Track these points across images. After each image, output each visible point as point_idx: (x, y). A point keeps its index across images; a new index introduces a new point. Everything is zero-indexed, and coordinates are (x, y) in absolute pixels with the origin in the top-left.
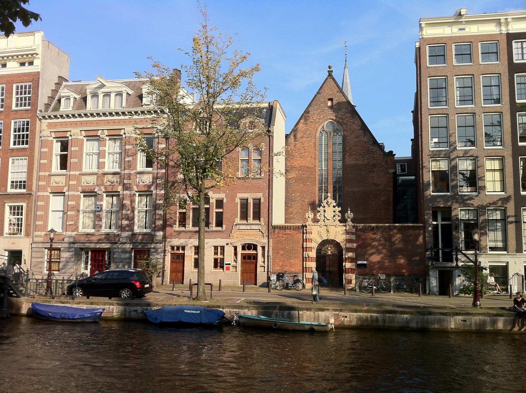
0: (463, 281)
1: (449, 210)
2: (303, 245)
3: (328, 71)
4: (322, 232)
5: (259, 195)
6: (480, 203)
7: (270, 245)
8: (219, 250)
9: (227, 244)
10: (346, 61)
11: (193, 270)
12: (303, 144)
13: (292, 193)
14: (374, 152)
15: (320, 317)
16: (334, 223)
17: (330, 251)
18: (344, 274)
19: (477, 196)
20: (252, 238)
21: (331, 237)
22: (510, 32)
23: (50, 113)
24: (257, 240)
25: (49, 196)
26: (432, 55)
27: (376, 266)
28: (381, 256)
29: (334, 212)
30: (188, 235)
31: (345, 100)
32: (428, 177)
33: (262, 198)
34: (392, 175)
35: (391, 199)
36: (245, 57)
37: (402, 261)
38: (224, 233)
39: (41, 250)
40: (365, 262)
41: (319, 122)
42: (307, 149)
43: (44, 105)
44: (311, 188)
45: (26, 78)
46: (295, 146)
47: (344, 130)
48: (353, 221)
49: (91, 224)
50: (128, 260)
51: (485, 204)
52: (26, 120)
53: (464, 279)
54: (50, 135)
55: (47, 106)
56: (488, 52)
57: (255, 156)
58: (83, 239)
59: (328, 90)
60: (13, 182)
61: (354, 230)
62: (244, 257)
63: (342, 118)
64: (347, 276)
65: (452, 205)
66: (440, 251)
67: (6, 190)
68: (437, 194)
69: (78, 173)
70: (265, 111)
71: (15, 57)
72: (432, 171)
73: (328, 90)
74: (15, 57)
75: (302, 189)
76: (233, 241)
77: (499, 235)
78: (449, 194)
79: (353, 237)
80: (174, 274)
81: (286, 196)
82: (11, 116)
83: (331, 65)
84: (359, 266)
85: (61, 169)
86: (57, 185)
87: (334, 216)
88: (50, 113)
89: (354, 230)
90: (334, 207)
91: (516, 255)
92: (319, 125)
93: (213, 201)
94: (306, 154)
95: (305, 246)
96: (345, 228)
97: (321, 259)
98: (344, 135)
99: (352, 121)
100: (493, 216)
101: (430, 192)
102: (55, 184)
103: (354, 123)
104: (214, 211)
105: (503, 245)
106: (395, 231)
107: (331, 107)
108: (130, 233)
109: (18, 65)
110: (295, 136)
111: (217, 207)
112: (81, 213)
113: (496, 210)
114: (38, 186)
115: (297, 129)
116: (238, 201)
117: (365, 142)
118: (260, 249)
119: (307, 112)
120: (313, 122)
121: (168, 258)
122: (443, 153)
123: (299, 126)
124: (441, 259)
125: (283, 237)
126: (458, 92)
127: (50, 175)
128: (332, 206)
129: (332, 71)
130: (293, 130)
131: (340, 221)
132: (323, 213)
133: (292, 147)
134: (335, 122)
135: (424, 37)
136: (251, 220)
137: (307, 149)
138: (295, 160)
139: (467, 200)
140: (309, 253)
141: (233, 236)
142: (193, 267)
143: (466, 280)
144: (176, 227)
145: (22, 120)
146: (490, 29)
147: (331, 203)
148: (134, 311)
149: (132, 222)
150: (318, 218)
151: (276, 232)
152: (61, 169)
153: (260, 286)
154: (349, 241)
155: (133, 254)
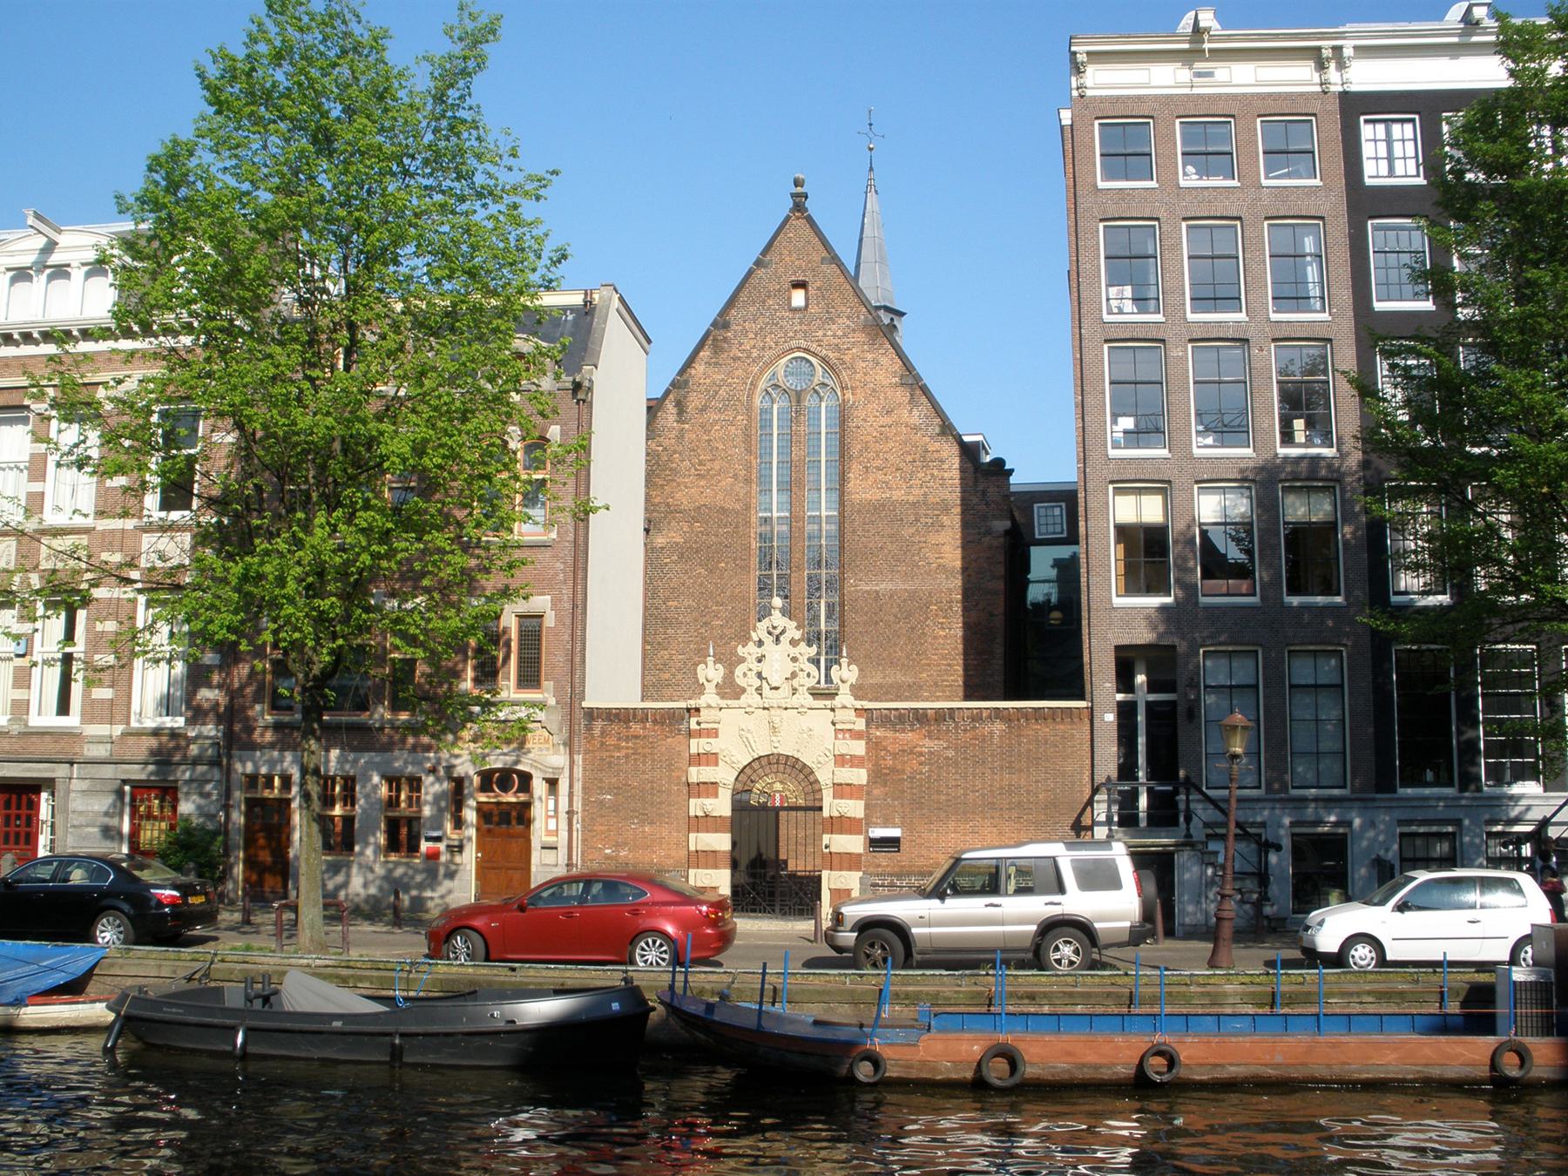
3: (793, 195)
7: (575, 775)
10: (871, 169)
13: (668, 599)
14: (942, 461)
17: (779, 790)
21: (786, 747)
22: (1354, 88)
26: (1112, 151)
29: (794, 659)
33: (548, 611)
34: (1002, 540)
35: (999, 621)
41: (759, 357)
42: (721, 447)
44: (735, 582)
46: (680, 437)
48: (858, 691)
56: (1283, 147)
59: (790, 255)
63: (837, 348)
70: (570, 317)
73: (790, 255)
75: (701, 585)
78: (1339, 599)
81: (646, 609)
83: (801, 176)
84: (877, 844)
87: (794, 675)
90: (794, 643)
91: (1373, 800)
96: (700, 719)
99: (869, 356)
103: (878, 363)
115: (686, 382)
117: (916, 428)
118: (539, 787)
120: (739, 358)
123: (693, 372)
125: (619, 748)
128: (785, 639)
130: (673, 384)
131: (816, 694)
133: (669, 440)
135: (1089, 93)
137: (721, 447)
138: (679, 484)
146: (1297, 77)
147: (783, 632)
150: (740, 681)
151: (597, 732)
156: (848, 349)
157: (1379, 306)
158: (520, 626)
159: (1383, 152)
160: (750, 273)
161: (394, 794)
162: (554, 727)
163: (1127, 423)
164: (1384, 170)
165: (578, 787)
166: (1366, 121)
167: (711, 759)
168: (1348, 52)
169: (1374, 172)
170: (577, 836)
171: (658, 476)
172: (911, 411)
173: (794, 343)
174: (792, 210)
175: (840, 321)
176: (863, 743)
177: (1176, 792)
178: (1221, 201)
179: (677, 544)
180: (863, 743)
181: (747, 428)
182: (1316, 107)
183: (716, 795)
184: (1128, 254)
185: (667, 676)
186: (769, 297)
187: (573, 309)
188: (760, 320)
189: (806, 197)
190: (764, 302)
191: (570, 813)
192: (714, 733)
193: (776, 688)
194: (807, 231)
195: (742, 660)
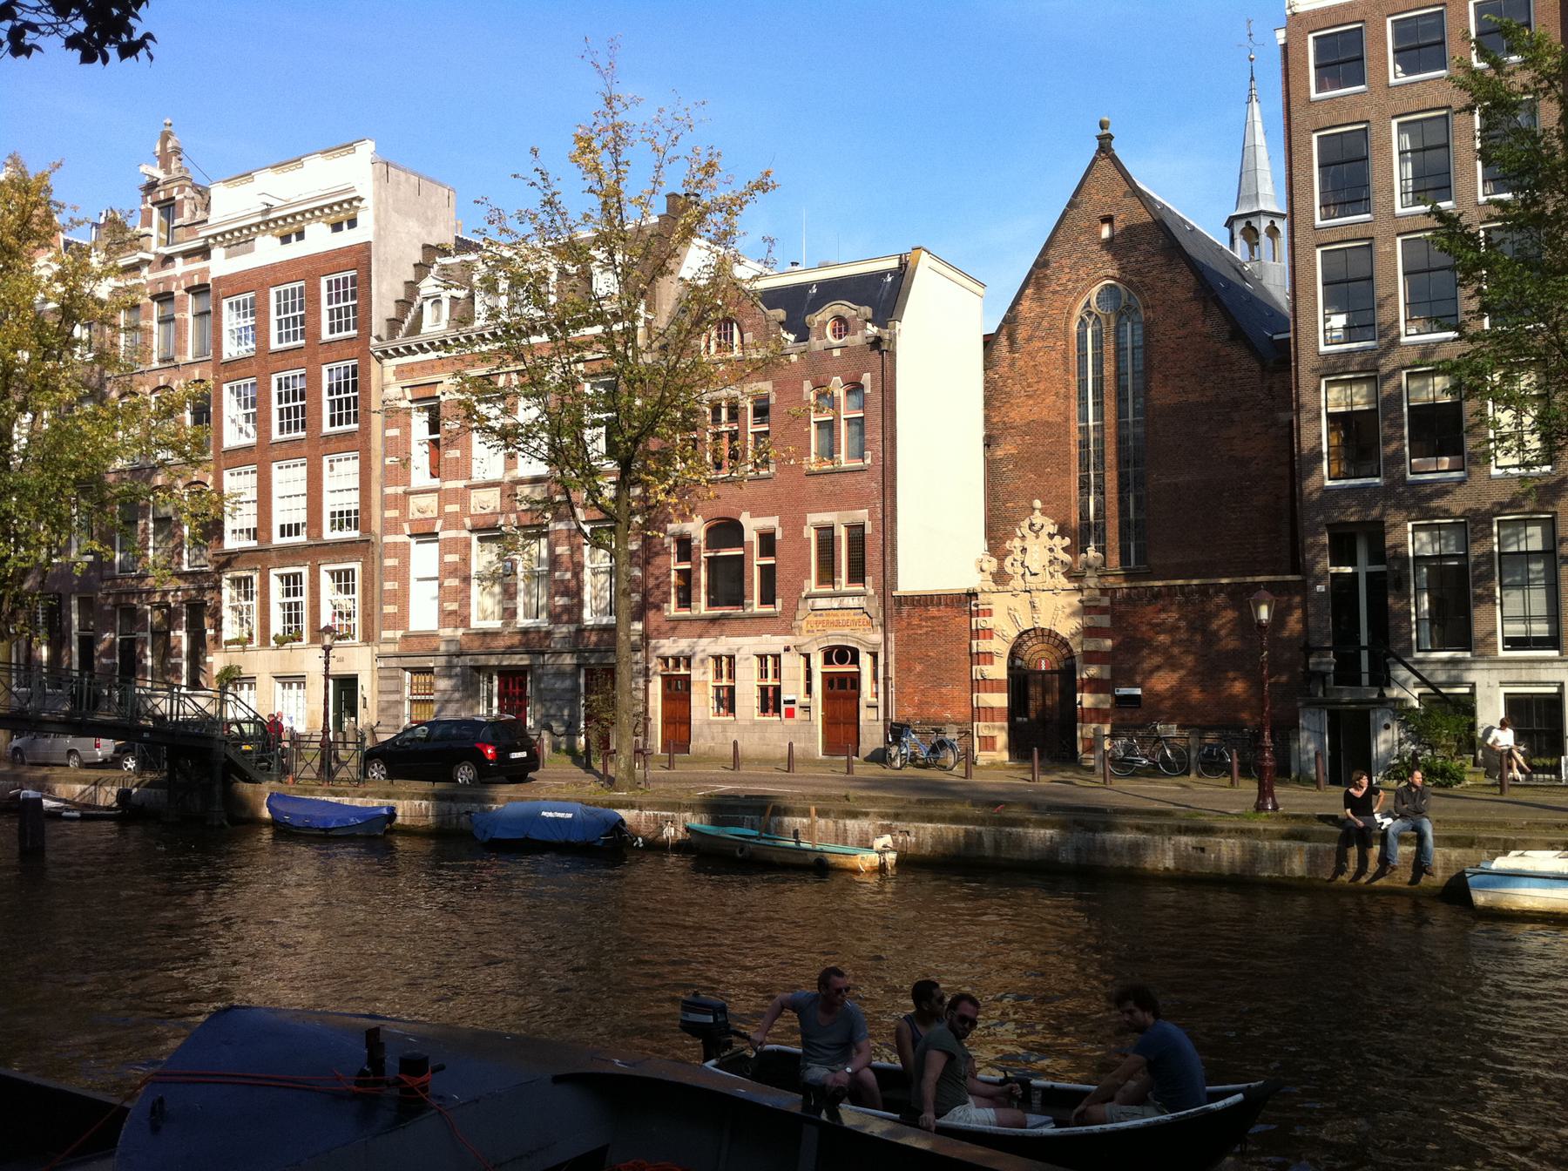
0: (1401, 742)
1: (1376, 532)
2: (970, 645)
3: (1099, 138)
4: (1018, 608)
5: (862, 515)
6: (1471, 505)
8: (769, 663)
9: (787, 649)
10: (1252, 79)
11: (756, 718)
12: (1033, 358)
13: (1006, 501)
14: (1232, 364)
15: (849, 833)
16: (1050, 583)
17: (1042, 660)
18: (1079, 724)
19: (1461, 482)
20: (846, 631)
21: (1044, 623)
23: (401, 340)
24: (858, 635)
25: (407, 544)
27: (1168, 703)
28: (1183, 672)
29: (1051, 550)
30: (698, 627)
31: (1146, 218)
32: (1320, 436)
36: (711, 165)
37: (1238, 687)
38: (780, 621)
39: (394, 674)
40: (1138, 691)
41: (1074, 288)
42: (1045, 370)
43: (385, 324)
45: (343, 261)
46: (1012, 365)
47: (1146, 307)
49: (497, 610)
50: (568, 696)
51: (1488, 506)
52: (350, 363)
53: (1402, 735)
54: (401, 395)
55: (394, 324)
57: (847, 410)
58: (476, 645)
60: (333, 514)
61: (1106, 602)
62: (828, 679)
63: (1138, 272)
64: (1085, 731)
65: (1383, 514)
66: (1364, 655)
67: (269, 540)
68: (1342, 482)
69: (461, 484)
70: (889, 279)
71: (317, 213)
72: (1332, 417)
74: (317, 213)
76: (800, 640)
77: (1538, 600)
78: (1377, 480)
79: (1105, 621)
80: (672, 728)
82: (321, 357)
83: (1106, 119)
84: (1121, 701)
85: (433, 476)
86: (422, 516)
88: (401, 340)
90: (1051, 536)
92: (1076, 300)
93: (751, 535)
94: (1042, 386)
95: (974, 650)
97: (1020, 681)
99: (1167, 276)
100: (1518, 542)
101: (1325, 477)
102: (418, 515)
104: (757, 561)
105: (1550, 632)
106: (1221, 599)
107: (1108, 244)
108: (572, 628)
109: (278, 241)
110: (1012, 339)
111: (763, 554)
112: (474, 583)
113: (1526, 523)
114: (384, 521)
115: (1015, 317)
116: (812, 534)
118: (865, 661)
119: (1041, 264)
120: (1057, 292)
121: (656, 687)
122: (1358, 359)
123: (1021, 308)
124: (1365, 679)
125: (921, 627)
126: (1410, 165)
127: (407, 494)
129: (1111, 137)
130: (1004, 320)
132: (1018, 555)
133: (1003, 369)
134: (1120, 286)
136: (843, 583)
138: (1012, 405)
139: (1430, 497)
140: (984, 667)
141: (800, 628)
142: (756, 711)
143: (1408, 739)
144: (672, 609)
145: (342, 364)
148: (467, 813)
149: (575, 601)
150: (1009, 569)
151: (905, 614)
152: (433, 476)
153: (867, 759)
154: (1089, 632)
155: (582, 681)
156: (1149, 272)
162: (872, 612)
165: (892, 659)
167: (988, 633)
170: (892, 697)
171: (996, 400)
172: (1204, 322)
173: (1102, 273)
174: (1098, 152)
175: (1142, 247)
176: (1108, 617)
178: (1431, 93)
179: (1012, 455)
180: (1108, 617)
181: (1066, 352)
183: (992, 663)
187: (891, 272)
191: (886, 679)
192: (989, 613)
193: (1036, 574)
194: (1112, 171)
195: (1010, 552)
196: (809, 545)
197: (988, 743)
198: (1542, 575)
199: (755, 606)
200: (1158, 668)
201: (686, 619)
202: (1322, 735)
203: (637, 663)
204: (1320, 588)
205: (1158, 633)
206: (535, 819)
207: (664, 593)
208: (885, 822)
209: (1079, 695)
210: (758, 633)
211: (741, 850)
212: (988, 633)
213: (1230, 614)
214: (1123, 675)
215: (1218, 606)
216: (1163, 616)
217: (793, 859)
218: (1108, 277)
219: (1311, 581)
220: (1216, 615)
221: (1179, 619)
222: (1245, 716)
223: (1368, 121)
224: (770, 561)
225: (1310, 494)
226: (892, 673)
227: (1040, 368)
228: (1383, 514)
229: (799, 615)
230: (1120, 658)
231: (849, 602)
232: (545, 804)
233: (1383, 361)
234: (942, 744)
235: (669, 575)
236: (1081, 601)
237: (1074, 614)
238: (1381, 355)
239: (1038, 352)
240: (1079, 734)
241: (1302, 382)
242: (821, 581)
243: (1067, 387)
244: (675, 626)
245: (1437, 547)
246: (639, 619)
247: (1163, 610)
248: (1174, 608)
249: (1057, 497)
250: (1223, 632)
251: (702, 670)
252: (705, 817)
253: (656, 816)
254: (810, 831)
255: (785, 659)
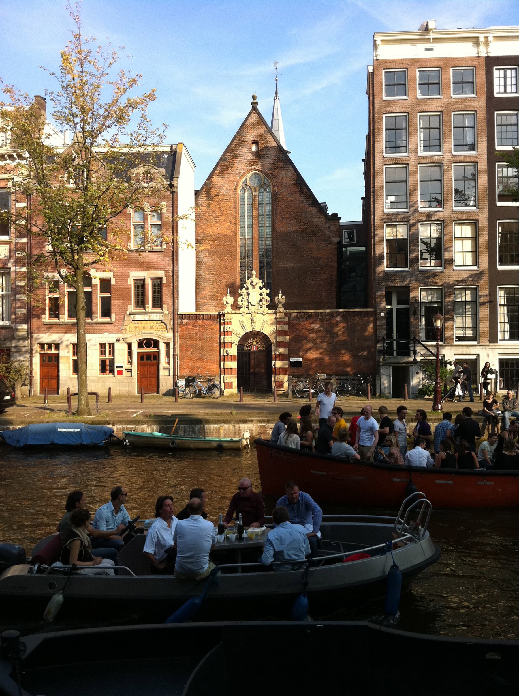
2: (220, 339)
3: (252, 103)
5: (160, 274)
9: (118, 340)
10: (276, 89)
12: (219, 204)
13: (205, 271)
14: (313, 215)
16: (261, 310)
17: (255, 346)
18: (273, 375)
19: (442, 272)
20: (152, 331)
21: (257, 329)
22: (491, 55)
24: (159, 333)
27: (314, 364)
29: (261, 295)
35: (335, 278)
37: (346, 357)
38: (114, 326)
40: (301, 360)
42: (225, 210)
44: (231, 264)
46: (208, 206)
48: (285, 306)
51: (452, 282)
57: (153, 220)
59: (251, 129)
61: (287, 319)
62: (141, 357)
63: (270, 169)
65: (409, 284)
68: (392, 269)
70: (166, 157)
72: (387, 240)
75: (218, 265)
76: (125, 336)
77: (469, 321)
78: (407, 269)
79: (286, 328)
80: (46, 381)
81: (197, 275)
89: (287, 319)
90: (261, 288)
93: (96, 282)
94: (223, 218)
98: (274, 191)
99: (284, 172)
100: (461, 297)
101: (384, 267)
104: (99, 295)
105: (473, 334)
106: (338, 319)
107: (256, 154)
110: (208, 193)
113: (466, 289)
115: (210, 183)
116: (131, 281)
117: (302, 202)
118: (162, 347)
119: (223, 159)
121: (36, 360)
123: (213, 179)
125: (193, 330)
129: (257, 103)
130: (205, 184)
131: (269, 307)
132: (245, 297)
134: (261, 174)
136: (149, 308)
137: (225, 210)
138: (208, 225)
139: (429, 277)
140: (228, 349)
141: (126, 330)
142: (99, 372)
143: (426, 378)
144: (46, 318)
147: (256, 284)
150: (240, 303)
153: (164, 395)
154: (279, 333)
156: (276, 169)
157: (498, 148)
158: (152, 283)
159: (502, 83)
160: (235, 137)
161: (76, 350)
162: (167, 322)
163: (392, 198)
164: (502, 90)
165: (177, 346)
166: (496, 69)
167: (230, 333)
168: (490, 39)
169: (498, 92)
173: (253, 167)
175: (272, 157)
177: (409, 343)
179: (208, 249)
182: (476, 63)
184: (394, 127)
185: (205, 301)
186: (243, 147)
188: (240, 157)
189: (258, 104)
190: (241, 149)
192: (231, 323)
193: (254, 306)
195: (241, 295)
196: (131, 288)
197: (229, 385)
198: (470, 309)
199: (98, 318)
200: (310, 349)
201: (56, 324)
202: (390, 376)
203: (25, 347)
204: (383, 314)
205: (310, 333)
206: (54, 431)
207: (42, 309)
208: (262, 424)
209: (273, 362)
210: (101, 332)
211: (173, 444)
212: (230, 333)
213: (342, 325)
214: (293, 351)
215: (337, 321)
216: (313, 325)
217: (203, 446)
218: (256, 169)
219: (378, 311)
220: (337, 325)
221: (320, 327)
222: (349, 369)
223: (408, 113)
224: (108, 295)
225: (379, 273)
226: (177, 352)
227: (222, 209)
228: (409, 284)
229: (125, 323)
230: (293, 344)
231: (154, 317)
232: (58, 424)
233: (411, 218)
234: (214, 386)
235: (45, 300)
236: (276, 318)
237: (272, 324)
238: (411, 215)
239: (222, 201)
240: (273, 379)
241: (376, 224)
242: (137, 305)
243: (236, 219)
244: (49, 328)
245: (429, 298)
246: (26, 323)
247: (312, 323)
248: (318, 322)
249: (231, 270)
250: (340, 333)
251: (66, 351)
252: (155, 427)
253: (123, 428)
254: (218, 431)
255: (117, 346)
